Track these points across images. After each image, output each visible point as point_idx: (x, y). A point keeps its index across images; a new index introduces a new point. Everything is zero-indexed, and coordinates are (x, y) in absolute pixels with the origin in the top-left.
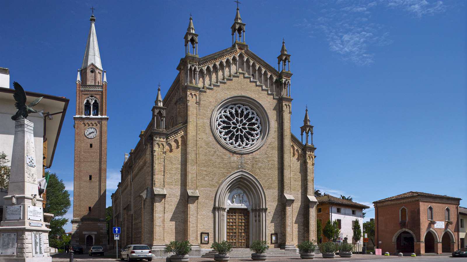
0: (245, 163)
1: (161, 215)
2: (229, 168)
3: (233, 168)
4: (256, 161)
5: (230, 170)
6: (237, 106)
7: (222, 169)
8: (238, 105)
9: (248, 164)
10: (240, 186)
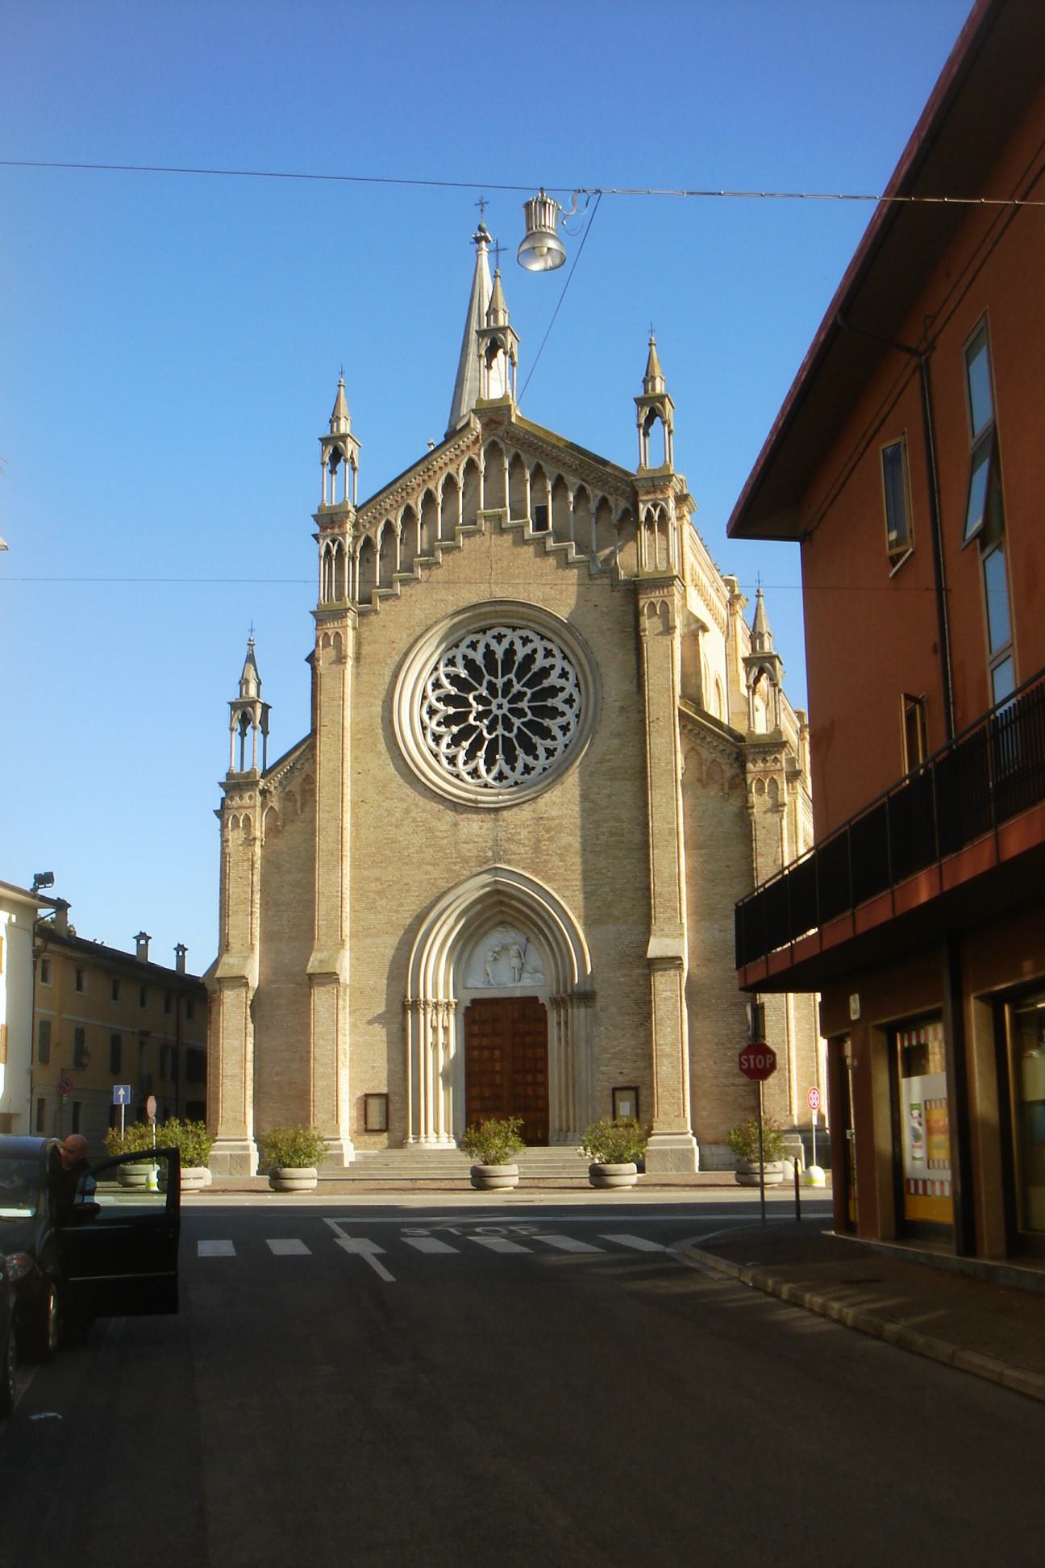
0: (508, 840)
1: (236, 1043)
2: (455, 864)
3: (465, 860)
4: (548, 830)
5: (457, 868)
6: (490, 633)
7: (430, 868)
8: (495, 632)
9: (519, 842)
10: (509, 919)
